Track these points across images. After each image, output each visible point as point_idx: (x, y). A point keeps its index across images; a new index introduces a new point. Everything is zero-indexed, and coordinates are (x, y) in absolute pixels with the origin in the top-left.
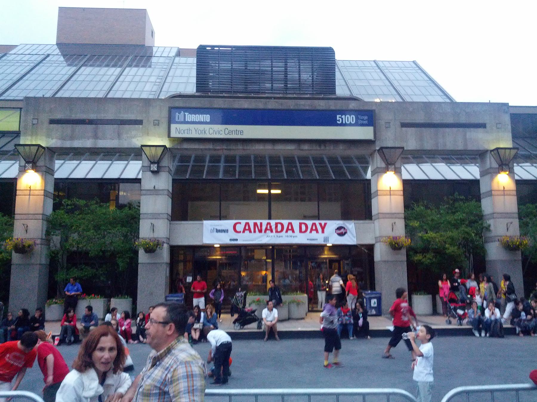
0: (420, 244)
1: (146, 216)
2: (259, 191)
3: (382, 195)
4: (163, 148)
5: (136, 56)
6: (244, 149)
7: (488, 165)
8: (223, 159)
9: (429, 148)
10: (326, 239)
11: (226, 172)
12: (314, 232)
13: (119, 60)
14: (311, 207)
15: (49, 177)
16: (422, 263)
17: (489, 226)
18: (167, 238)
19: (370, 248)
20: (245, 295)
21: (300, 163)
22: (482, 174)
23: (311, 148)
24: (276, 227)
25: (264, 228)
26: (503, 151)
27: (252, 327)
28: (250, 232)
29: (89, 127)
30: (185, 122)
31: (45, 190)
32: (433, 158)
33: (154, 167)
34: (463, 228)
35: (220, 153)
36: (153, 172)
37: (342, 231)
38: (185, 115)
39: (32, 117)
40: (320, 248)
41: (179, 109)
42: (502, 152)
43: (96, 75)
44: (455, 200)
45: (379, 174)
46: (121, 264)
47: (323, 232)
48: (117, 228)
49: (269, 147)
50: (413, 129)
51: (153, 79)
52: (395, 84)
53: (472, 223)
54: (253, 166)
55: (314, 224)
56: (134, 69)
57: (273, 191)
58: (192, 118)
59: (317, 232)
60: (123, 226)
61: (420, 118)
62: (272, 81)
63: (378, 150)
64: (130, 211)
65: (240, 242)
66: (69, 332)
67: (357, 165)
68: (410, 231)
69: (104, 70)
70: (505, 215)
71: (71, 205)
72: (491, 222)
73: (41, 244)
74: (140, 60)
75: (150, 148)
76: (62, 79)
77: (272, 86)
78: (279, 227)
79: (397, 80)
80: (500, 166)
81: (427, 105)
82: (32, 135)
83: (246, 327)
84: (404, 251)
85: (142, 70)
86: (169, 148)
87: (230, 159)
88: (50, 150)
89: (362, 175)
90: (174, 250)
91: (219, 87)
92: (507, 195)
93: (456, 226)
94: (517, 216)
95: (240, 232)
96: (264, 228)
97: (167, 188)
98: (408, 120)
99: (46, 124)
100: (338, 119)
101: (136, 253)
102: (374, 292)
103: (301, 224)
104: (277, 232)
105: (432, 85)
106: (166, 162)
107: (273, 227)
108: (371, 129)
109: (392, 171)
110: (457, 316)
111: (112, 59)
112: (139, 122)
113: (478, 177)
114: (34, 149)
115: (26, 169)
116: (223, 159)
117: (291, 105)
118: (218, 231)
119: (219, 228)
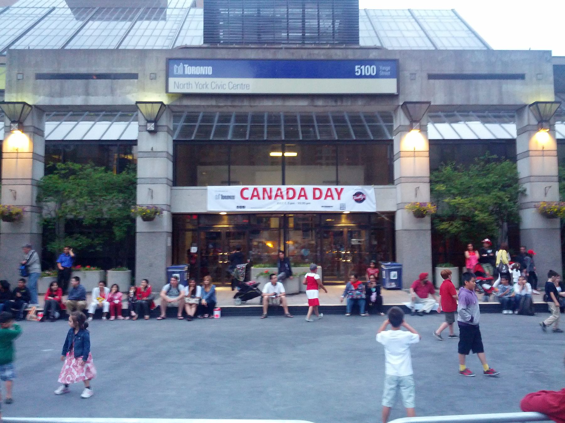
0: (447, 211)
1: (143, 181)
2: (273, 154)
3: (404, 157)
4: (160, 105)
5: (148, 8)
6: (251, 106)
7: (526, 123)
8: (233, 119)
9: (459, 103)
10: (343, 206)
11: (235, 134)
12: (329, 199)
13: (130, 12)
14: (329, 171)
15: (38, 138)
16: (448, 232)
17: (525, 190)
18: (167, 205)
19: (392, 215)
20: (248, 269)
21: (318, 123)
22: (520, 132)
23: (326, 104)
24: (287, 193)
25: (274, 194)
26: (544, 105)
27: (254, 302)
28: (259, 199)
29: (79, 82)
30: (184, 76)
31: (33, 153)
32: (468, 116)
33: (151, 127)
34: (496, 192)
35: (231, 109)
36: (150, 132)
37: (360, 197)
38: (184, 67)
39: (16, 72)
40: (337, 215)
41: (178, 60)
42: (541, 106)
43: (104, 30)
44: (488, 161)
45: (403, 132)
47: (339, 198)
48: (113, 194)
49: (279, 103)
50: (442, 81)
51: (165, 33)
52: (431, 34)
53: (504, 188)
54: (266, 127)
55: (329, 189)
56: (146, 23)
57: (287, 154)
58: (193, 70)
59: (333, 199)
60: (121, 191)
61: (450, 69)
62: (288, 29)
63: (402, 105)
64: (128, 176)
65: (248, 209)
66: (53, 306)
67: (382, 124)
69: (113, 24)
70: (543, 178)
71: (64, 169)
72: (527, 186)
73: (32, 212)
74: (152, 13)
75: (146, 106)
76: (68, 34)
77: (288, 35)
78: (291, 192)
79: (434, 31)
80: (539, 122)
81: (458, 54)
82: (17, 92)
83: (249, 301)
84: (428, 219)
85: (154, 23)
86: (168, 105)
87: (241, 118)
88: (40, 109)
89: (386, 136)
91: (228, 37)
93: (487, 190)
94: (556, 179)
95: (247, 199)
96: (274, 194)
97: (165, 150)
98: (436, 71)
100: (356, 70)
101: (134, 221)
102: (394, 264)
105: (472, 35)
106: (164, 121)
107: (284, 193)
108: (394, 81)
109: (416, 129)
110: (482, 291)
111: (122, 12)
112: (134, 76)
113: (515, 136)
114: (19, 107)
115: (12, 129)
116: (233, 119)
117: (304, 55)
118: (224, 197)
119: (224, 194)
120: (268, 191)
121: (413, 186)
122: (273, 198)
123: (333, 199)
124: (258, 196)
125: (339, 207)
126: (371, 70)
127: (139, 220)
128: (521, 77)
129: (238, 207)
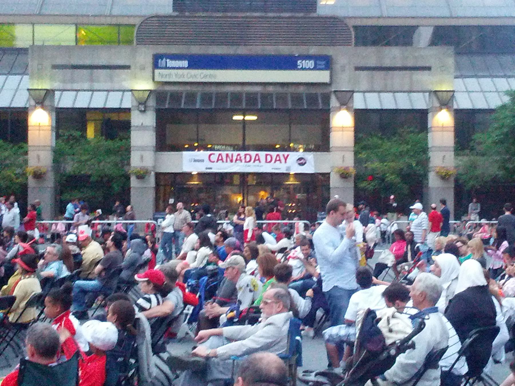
10: (288, 168)
12: (278, 162)
19: (326, 176)
24: (245, 158)
25: (234, 158)
28: (223, 162)
29: (85, 72)
30: (166, 68)
34: (407, 159)
38: (166, 62)
40: (286, 175)
46: (116, 188)
47: (286, 162)
57: (248, 118)
59: (281, 162)
68: (357, 161)
78: (248, 157)
90: (158, 175)
92: (445, 131)
95: (214, 162)
96: (234, 158)
98: (362, 64)
99: (49, 69)
103: (267, 155)
104: (246, 162)
107: (243, 158)
112: (128, 67)
118: (195, 161)
119: (196, 158)
120: (230, 156)
121: (442, 154)
122: (234, 161)
123: (281, 162)
124: (222, 159)
125: (285, 169)
126: (311, 64)
127: (133, 179)
128: (429, 68)
129: (207, 168)
